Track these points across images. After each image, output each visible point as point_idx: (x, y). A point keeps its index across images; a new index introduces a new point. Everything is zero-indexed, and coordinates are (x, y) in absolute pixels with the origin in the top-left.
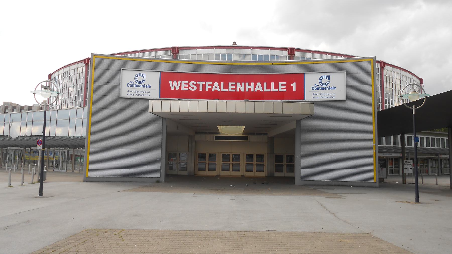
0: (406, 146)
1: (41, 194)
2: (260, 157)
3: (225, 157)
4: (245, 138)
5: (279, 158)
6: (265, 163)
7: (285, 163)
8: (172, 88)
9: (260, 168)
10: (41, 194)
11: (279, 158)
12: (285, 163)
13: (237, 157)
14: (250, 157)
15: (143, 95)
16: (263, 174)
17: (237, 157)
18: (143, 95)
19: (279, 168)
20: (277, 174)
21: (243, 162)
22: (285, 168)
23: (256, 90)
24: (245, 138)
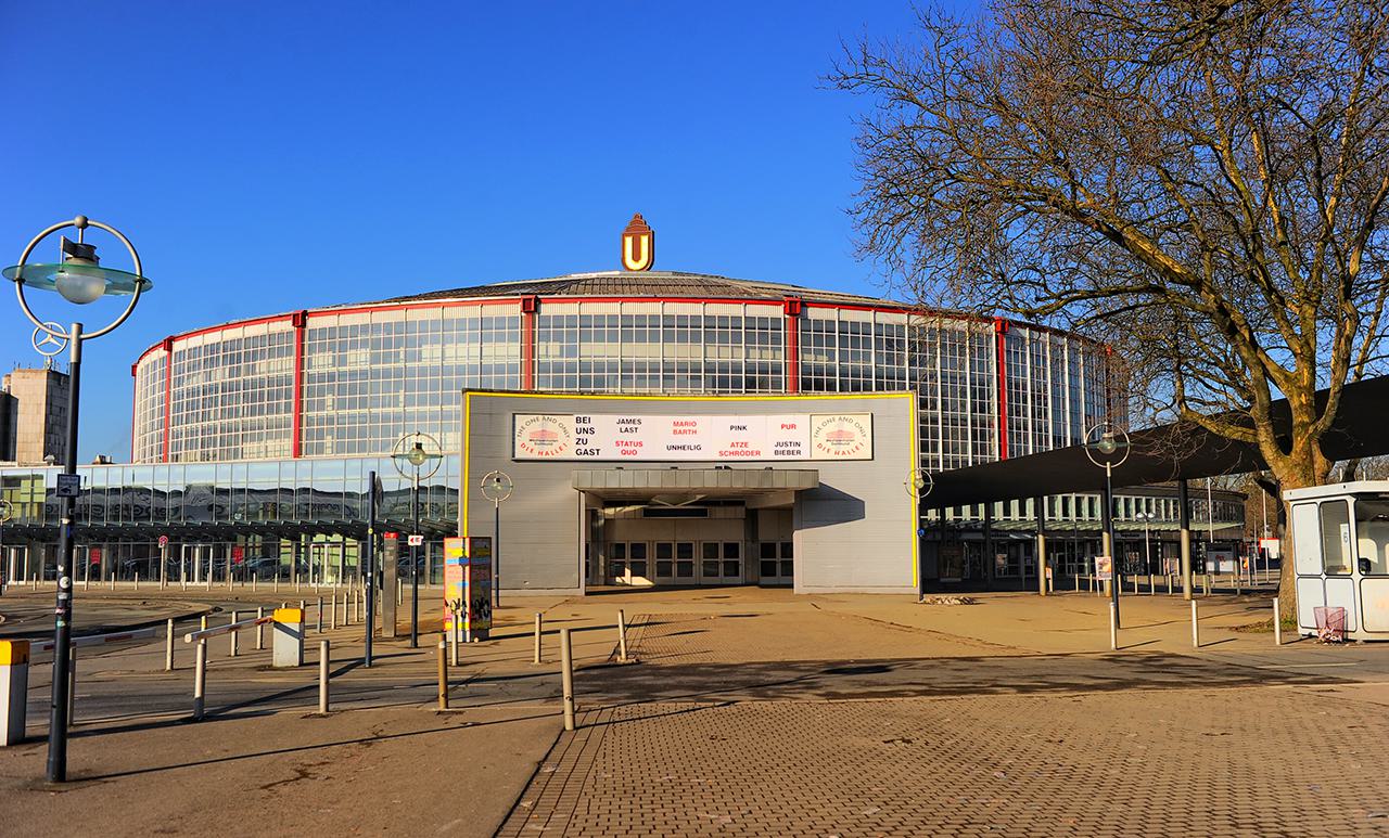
0: (1047, 518)
2: (731, 549)
3: (711, 550)
6: (741, 560)
11: (768, 549)
13: (685, 550)
14: (711, 550)
17: (685, 550)
21: (698, 559)
24: (703, 513)
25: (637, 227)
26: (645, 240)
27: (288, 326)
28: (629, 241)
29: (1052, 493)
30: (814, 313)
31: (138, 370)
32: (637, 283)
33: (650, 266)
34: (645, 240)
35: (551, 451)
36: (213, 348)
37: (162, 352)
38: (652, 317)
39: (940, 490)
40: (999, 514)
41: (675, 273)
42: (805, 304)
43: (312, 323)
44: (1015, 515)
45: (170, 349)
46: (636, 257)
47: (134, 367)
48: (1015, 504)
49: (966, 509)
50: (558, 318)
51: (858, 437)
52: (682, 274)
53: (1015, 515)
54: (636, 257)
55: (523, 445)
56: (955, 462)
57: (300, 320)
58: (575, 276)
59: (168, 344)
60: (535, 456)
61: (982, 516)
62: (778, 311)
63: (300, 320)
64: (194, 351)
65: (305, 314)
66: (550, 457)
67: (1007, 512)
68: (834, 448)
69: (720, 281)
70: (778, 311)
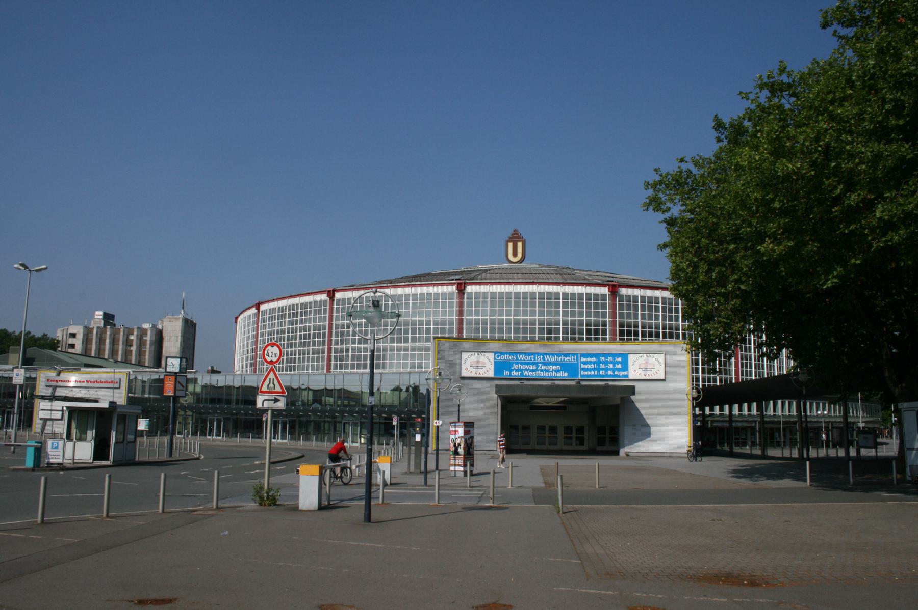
0: (808, 414)
1: (368, 518)
2: (580, 430)
3: (541, 428)
4: (564, 408)
5: (601, 430)
6: (586, 436)
7: (608, 435)
8: (97, 313)
9: (581, 441)
10: (368, 518)
11: (601, 430)
12: (608, 435)
13: (553, 429)
14: (568, 430)
15: (87, 400)
16: (584, 448)
17: (553, 429)
18: (87, 400)
19: (601, 442)
20: (599, 448)
21: (561, 434)
22: (608, 440)
23: (670, 283)
24: (564, 408)
25: (515, 238)
26: (520, 245)
27: (324, 297)
28: (510, 245)
29: (767, 400)
30: (624, 291)
31: (239, 320)
32: (518, 272)
33: (521, 261)
34: (520, 245)
35: (651, 375)
36: (282, 309)
37: (254, 310)
38: (531, 293)
39: (705, 397)
40: (736, 411)
41: (540, 265)
42: (334, 291)
43: (338, 295)
44: (745, 412)
45: (258, 309)
46: (515, 254)
47: (237, 318)
48: (745, 405)
49: (717, 408)
50: (477, 294)
51: (657, 367)
52: (546, 266)
53: (745, 412)
54: (515, 254)
55: (466, 369)
56: (726, 380)
57: (331, 294)
58: (480, 267)
59: (258, 306)
60: (473, 375)
61: (727, 412)
62: (605, 290)
63: (331, 294)
64: (272, 310)
65: (334, 291)
66: (481, 376)
67: (740, 410)
68: (474, 371)
69: (569, 271)
70: (605, 290)
